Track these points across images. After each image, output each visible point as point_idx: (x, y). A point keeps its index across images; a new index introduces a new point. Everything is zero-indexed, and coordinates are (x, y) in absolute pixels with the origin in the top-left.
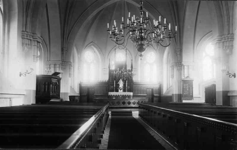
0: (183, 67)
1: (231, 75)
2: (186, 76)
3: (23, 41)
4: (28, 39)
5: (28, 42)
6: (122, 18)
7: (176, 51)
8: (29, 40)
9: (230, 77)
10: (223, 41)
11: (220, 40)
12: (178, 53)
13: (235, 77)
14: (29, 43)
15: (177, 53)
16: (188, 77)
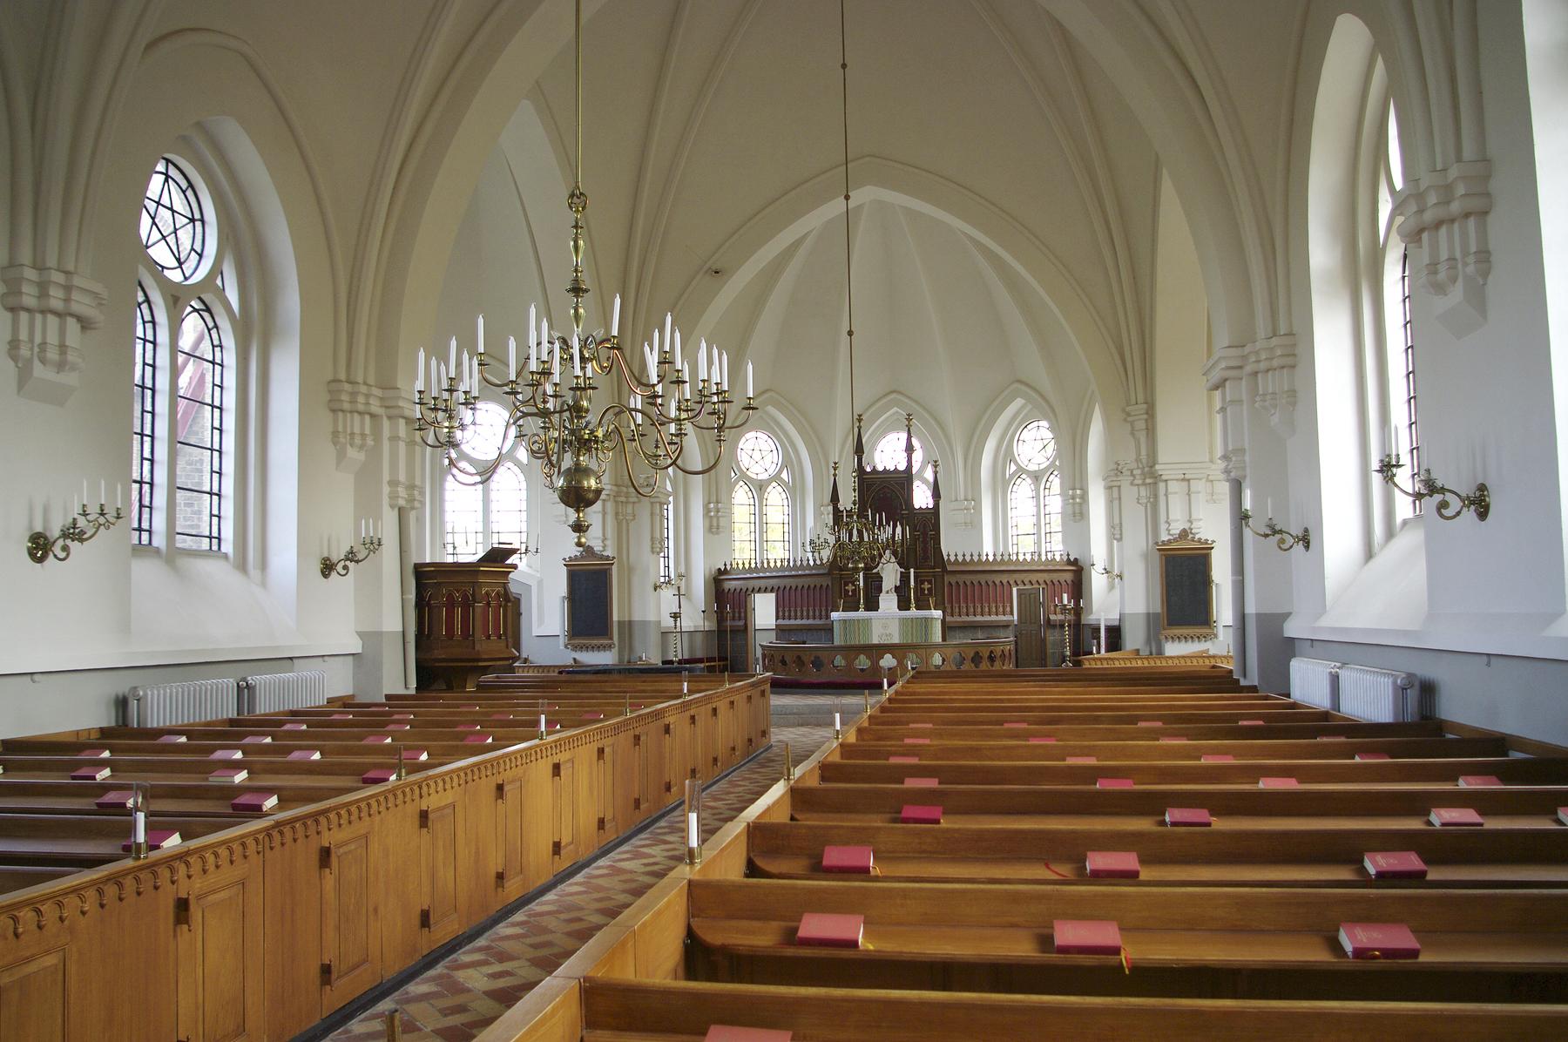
0: (1162, 486)
1: (1449, 497)
2: (1176, 529)
3: (335, 421)
4: (360, 413)
5: (362, 424)
6: (686, 822)
7: (1129, 414)
8: (367, 418)
9: (1441, 516)
10: (1249, 369)
11: (1240, 367)
12: (1141, 425)
13: (1483, 514)
14: (367, 431)
15: (1132, 423)
16: (1184, 534)
